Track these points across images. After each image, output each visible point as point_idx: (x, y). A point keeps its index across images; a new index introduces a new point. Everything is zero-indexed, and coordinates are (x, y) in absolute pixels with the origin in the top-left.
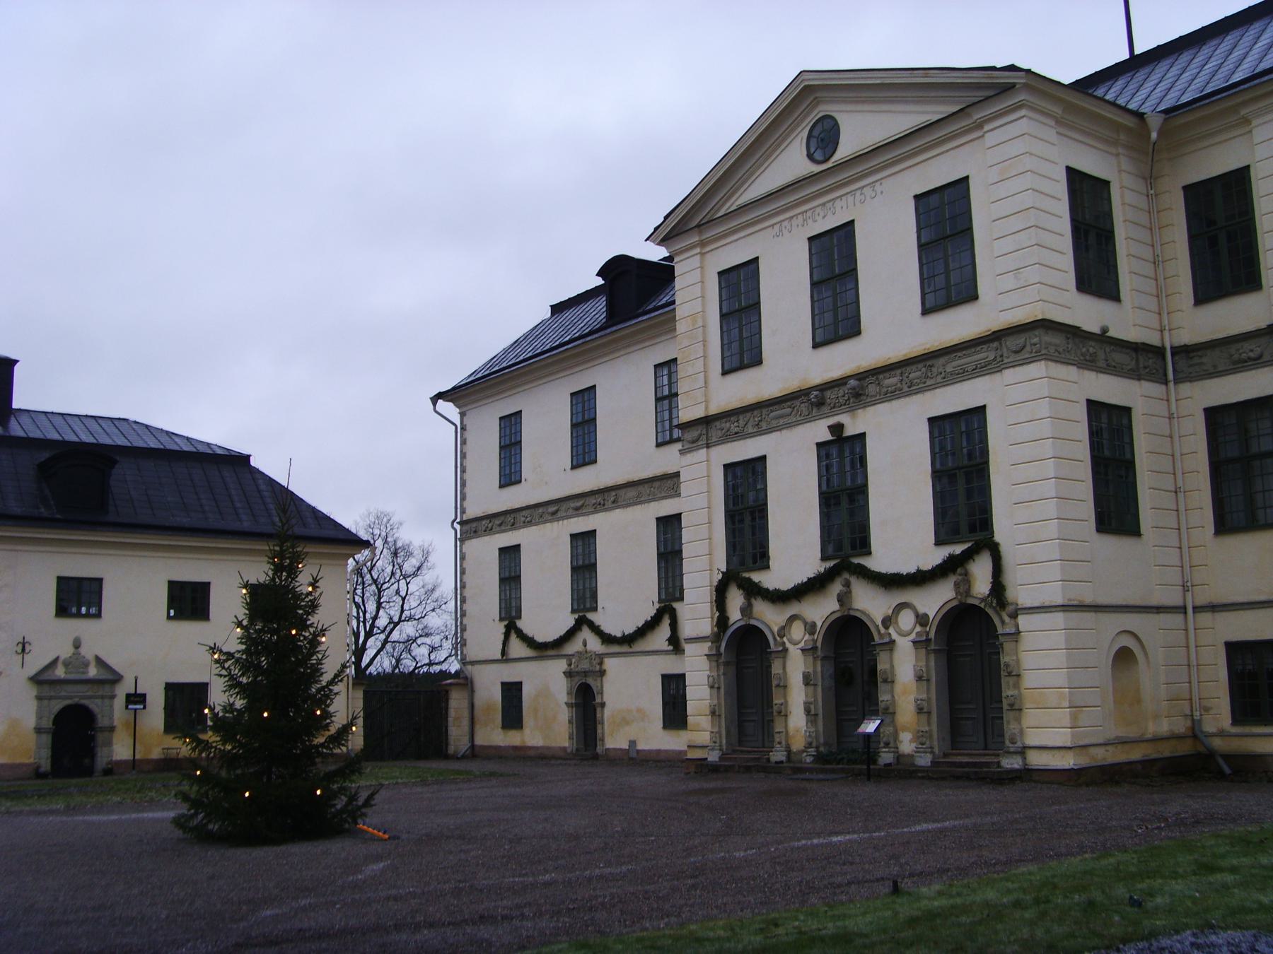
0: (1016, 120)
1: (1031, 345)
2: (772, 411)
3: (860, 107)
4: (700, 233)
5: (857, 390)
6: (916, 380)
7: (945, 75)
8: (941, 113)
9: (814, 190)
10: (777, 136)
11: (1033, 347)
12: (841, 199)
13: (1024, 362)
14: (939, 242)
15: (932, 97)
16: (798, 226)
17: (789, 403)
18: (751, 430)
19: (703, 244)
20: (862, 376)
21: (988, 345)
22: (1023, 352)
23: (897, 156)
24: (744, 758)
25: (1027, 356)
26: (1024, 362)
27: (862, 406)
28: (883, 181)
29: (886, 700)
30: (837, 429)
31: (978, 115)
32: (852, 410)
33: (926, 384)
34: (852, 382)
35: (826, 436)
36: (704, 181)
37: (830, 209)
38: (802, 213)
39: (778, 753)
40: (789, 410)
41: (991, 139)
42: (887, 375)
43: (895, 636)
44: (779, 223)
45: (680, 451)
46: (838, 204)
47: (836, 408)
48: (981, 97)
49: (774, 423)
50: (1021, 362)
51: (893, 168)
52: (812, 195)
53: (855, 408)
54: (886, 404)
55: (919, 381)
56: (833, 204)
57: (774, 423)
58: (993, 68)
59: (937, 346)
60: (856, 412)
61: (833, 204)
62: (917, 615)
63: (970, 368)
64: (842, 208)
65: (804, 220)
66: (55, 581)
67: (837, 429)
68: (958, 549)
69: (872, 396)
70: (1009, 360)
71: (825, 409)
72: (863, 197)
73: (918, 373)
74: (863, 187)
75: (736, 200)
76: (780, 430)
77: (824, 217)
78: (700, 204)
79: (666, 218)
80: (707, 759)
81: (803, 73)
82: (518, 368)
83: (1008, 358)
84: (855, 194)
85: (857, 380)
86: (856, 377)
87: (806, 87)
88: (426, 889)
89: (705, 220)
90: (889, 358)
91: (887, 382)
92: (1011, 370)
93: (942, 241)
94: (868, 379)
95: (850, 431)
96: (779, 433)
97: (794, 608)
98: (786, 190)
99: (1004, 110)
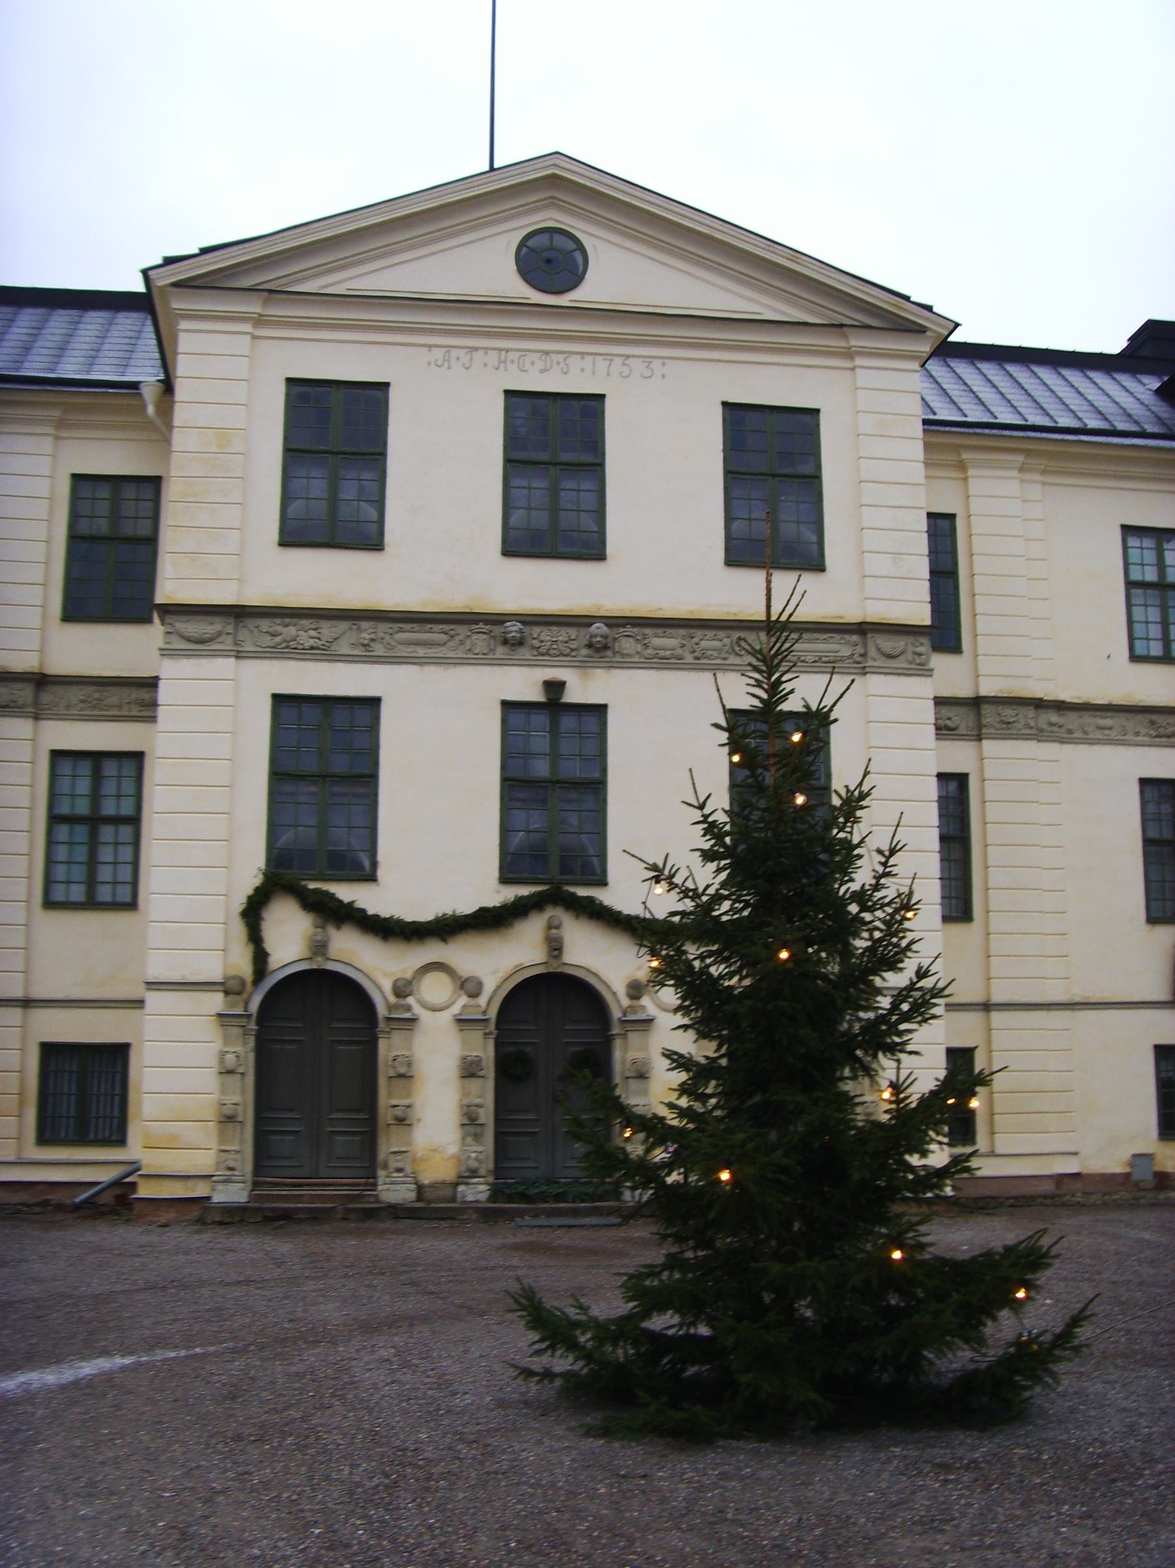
0: (307, 340)
1: (915, 653)
2: (401, 630)
3: (628, 244)
4: (266, 303)
5: (609, 640)
6: (711, 652)
7: (824, 272)
8: (790, 316)
9: (802, 342)
10: (656, 235)
11: (916, 657)
12: (486, 353)
13: (906, 672)
14: (765, 477)
15: (776, 288)
16: (429, 364)
17: (446, 627)
18: (345, 650)
19: (259, 321)
20: (617, 622)
21: (714, 632)
22: (900, 658)
23: (398, 322)
24: (566, 1202)
25: (903, 665)
26: (902, 671)
27: (606, 665)
28: (666, 361)
29: (642, 1104)
30: (554, 688)
31: (857, 341)
32: (583, 665)
33: (727, 662)
34: (599, 628)
35: (536, 695)
36: (309, 227)
37: (558, 363)
38: (500, 350)
39: (398, 1187)
40: (443, 637)
41: (863, 377)
42: (659, 631)
43: (417, 1010)
44: (447, 346)
45: (161, 649)
46: (575, 361)
47: (565, 656)
48: (858, 321)
49: (404, 651)
50: (899, 671)
51: (301, 331)
52: (654, 338)
53: (589, 665)
54: (652, 672)
55: (715, 654)
56: (565, 359)
57: (404, 651)
58: (907, 298)
59: (752, 615)
60: (590, 671)
61: (565, 359)
62: (409, 983)
63: (810, 658)
64: (583, 370)
65: (500, 362)
66: (610, 549)
67: (554, 688)
68: (525, 891)
69: (623, 655)
70: (876, 664)
71: (525, 653)
72: (626, 370)
73: (717, 644)
74: (477, 349)
75: (350, 279)
76: (421, 664)
77: (542, 371)
78: (279, 257)
79: (204, 251)
80: (208, 1198)
81: (557, 156)
82: (1062, 441)
83: (874, 660)
84: (611, 360)
85: (607, 625)
86: (605, 621)
87: (554, 177)
88: (85, 1552)
89: (266, 286)
90: (660, 609)
91: (657, 642)
92: (882, 677)
93: (770, 478)
94: (622, 630)
95: (573, 695)
96: (416, 668)
97: (432, 951)
98: (487, 306)
99: (754, 344)
